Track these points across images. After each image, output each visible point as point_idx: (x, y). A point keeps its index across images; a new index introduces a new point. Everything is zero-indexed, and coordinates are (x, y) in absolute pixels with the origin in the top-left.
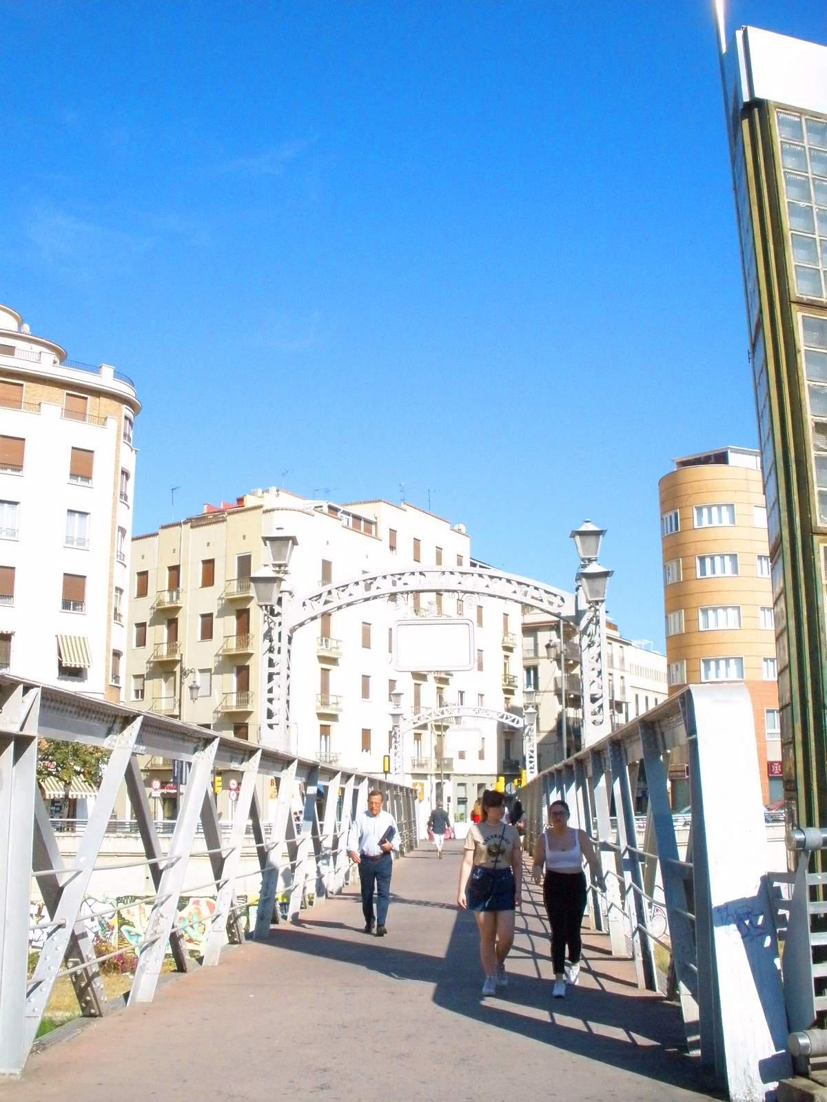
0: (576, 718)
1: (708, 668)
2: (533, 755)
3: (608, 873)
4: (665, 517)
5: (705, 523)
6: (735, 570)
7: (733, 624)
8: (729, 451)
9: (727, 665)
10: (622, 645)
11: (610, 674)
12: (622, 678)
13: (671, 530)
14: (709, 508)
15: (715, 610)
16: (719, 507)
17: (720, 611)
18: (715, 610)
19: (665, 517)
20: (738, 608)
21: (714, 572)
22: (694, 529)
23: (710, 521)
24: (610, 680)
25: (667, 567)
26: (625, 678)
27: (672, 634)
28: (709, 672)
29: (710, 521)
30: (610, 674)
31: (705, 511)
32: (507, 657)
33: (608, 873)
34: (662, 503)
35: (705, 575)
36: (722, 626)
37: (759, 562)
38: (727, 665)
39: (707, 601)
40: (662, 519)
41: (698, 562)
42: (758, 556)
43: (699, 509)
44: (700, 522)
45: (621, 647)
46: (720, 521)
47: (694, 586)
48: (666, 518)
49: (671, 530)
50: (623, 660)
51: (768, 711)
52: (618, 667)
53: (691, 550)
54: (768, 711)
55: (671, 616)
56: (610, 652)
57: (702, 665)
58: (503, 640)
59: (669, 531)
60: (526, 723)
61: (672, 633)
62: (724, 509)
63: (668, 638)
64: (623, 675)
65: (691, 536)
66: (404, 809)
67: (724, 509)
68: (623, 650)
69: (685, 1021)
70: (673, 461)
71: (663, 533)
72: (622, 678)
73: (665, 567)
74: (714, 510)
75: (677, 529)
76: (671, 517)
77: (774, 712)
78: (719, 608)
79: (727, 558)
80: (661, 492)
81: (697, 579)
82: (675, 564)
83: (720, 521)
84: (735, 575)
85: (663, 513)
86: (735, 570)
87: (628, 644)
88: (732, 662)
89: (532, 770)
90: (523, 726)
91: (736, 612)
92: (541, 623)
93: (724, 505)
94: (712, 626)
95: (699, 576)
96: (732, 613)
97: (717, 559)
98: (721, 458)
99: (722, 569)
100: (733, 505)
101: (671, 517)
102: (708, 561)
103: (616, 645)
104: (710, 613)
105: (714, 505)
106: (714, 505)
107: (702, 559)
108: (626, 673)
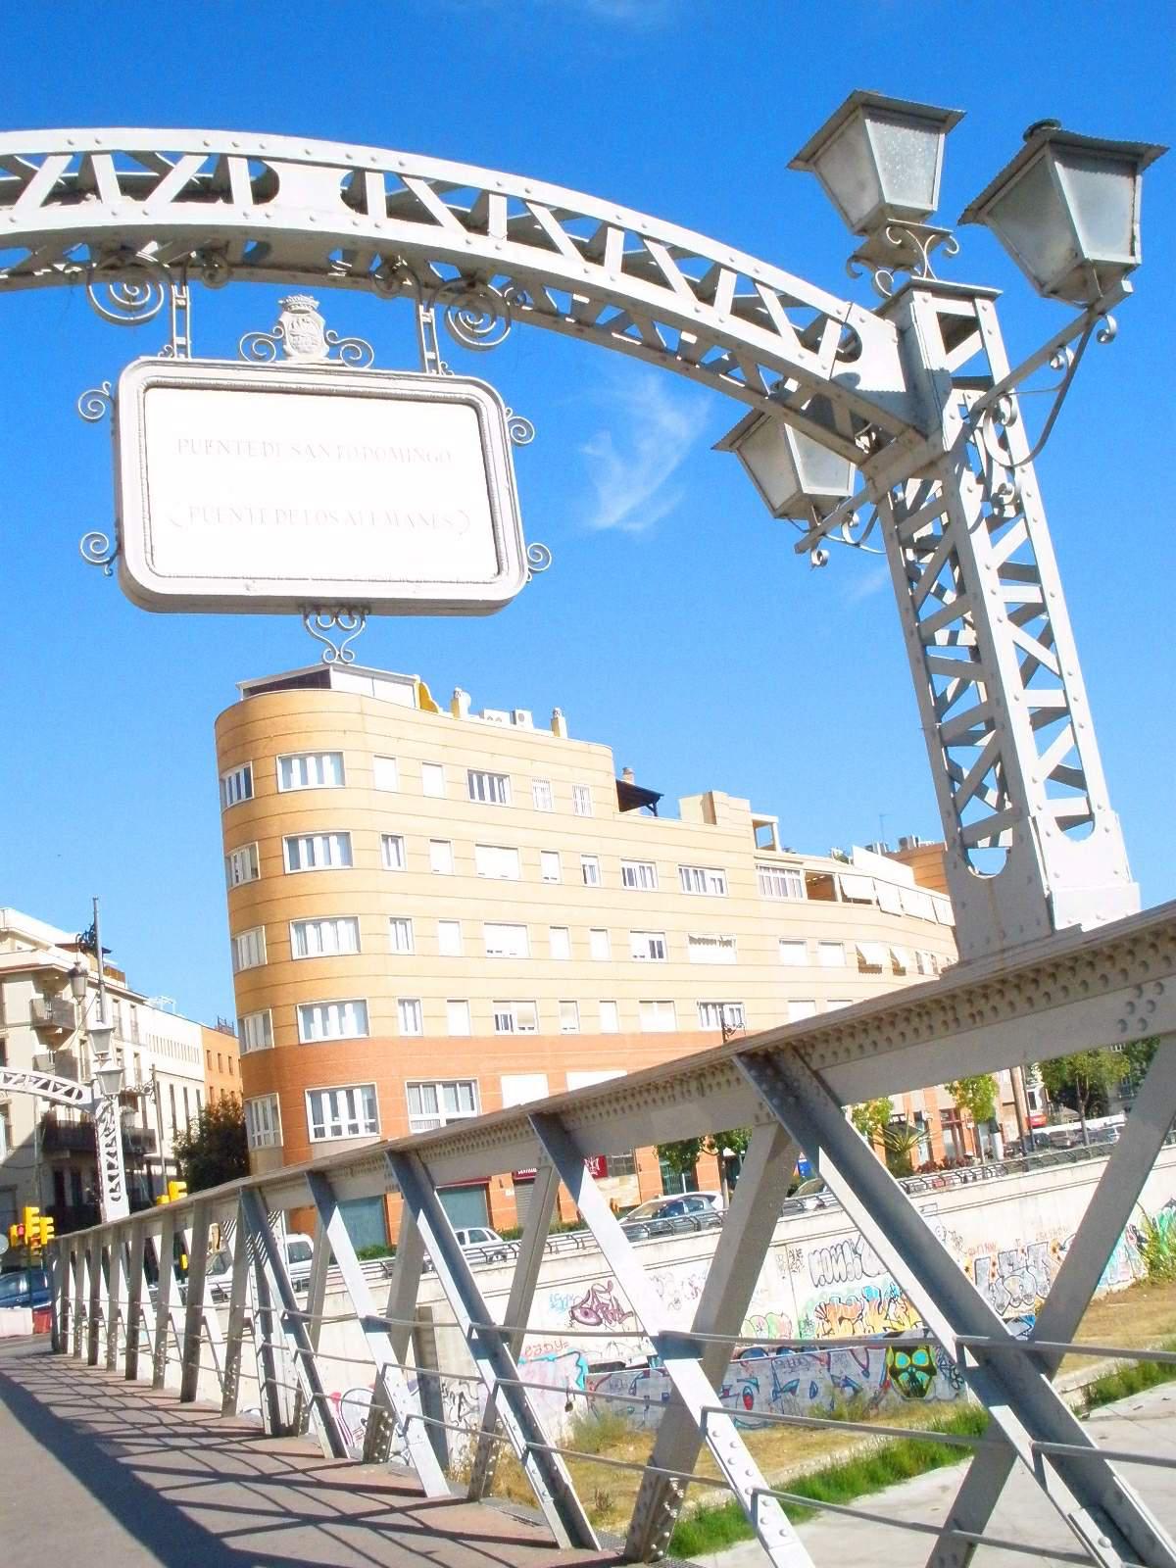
0: (70, 1121)
1: (309, 1019)
2: (110, 1159)
3: (754, 1497)
4: (226, 777)
5: (296, 783)
6: (348, 858)
7: (348, 946)
8: (331, 669)
9: (342, 1013)
10: (134, 1004)
11: (119, 1050)
12: (136, 1055)
13: (239, 797)
14: (303, 759)
15: (317, 923)
16: (319, 756)
17: (325, 926)
18: (317, 923)
19: (226, 777)
20: (355, 919)
21: (312, 862)
22: (279, 793)
23: (305, 779)
24: (119, 1060)
25: (233, 860)
26: (141, 1056)
27: (245, 967)
28: (312, 1025)
29: (305, 779)
30: (119, 1050)
31: (296, 763)
33: (754, 1497)
34: (223, 754)
35: (299, 868)
36: (330, 949)
37: (384, 845)
38: (342, 1013)
39: (305, 910)
40: (222, 781)
41: (286, 846)
42: (383, 835)
43: (287, 761)
44: (288, 783)
45: (133, 1007)
46: (321, 780)
47: (280, 887)
48: (230, 778)
49: (239, 797)
50: (136, 1026)
51: (411, 1086)
52: (130, 1039)
53: (274, 827)
54: (411, 1086)
55: (242, 939)
56: (116, 1014)
57: (300, 1015)
59: (228, 802)
60: (98, 1096)
61: (245, 965)
62: (326, 759)
63: (238, 974)
64: (137, 1052)
65: (274, 805)
66: (1056, 1448)
67: (326, 759)
68: (135, 1011)
69: (31, 982)
70: (238, 686)
71: (224, 802)
72: (136, 1055)
73: (228, 858)
74: (311, 761)
75: (249, 794)
76: (238, 776)
77: (418, 1087)
78: (339, 919)
79: (333, 840)
80: (219, 738)
81: (285, 875)
82: (247, 852)
83: (321, 780)
84: (348, 867)
85: (222, 771)
86: (348, 858)
87: (141, 1002)
88: (349, 1007)
89: (115, 1195)
90: (90, 1101)
91: (351, 925)
92: (12, 968)
93: (327, 753)
94: (313, 952)
95: (288, 870)
96: (345, 928)
97: (318, 842)
98: (318, 680)
99: (325, 856)
100: (341, 753)
101: (238, 776)
102: (302, 845)
103: (125, 1003)
104: (310, 928)
105: (310, 754)
106: (310, 754)
107: (293, 842)
108: (142, 1047)
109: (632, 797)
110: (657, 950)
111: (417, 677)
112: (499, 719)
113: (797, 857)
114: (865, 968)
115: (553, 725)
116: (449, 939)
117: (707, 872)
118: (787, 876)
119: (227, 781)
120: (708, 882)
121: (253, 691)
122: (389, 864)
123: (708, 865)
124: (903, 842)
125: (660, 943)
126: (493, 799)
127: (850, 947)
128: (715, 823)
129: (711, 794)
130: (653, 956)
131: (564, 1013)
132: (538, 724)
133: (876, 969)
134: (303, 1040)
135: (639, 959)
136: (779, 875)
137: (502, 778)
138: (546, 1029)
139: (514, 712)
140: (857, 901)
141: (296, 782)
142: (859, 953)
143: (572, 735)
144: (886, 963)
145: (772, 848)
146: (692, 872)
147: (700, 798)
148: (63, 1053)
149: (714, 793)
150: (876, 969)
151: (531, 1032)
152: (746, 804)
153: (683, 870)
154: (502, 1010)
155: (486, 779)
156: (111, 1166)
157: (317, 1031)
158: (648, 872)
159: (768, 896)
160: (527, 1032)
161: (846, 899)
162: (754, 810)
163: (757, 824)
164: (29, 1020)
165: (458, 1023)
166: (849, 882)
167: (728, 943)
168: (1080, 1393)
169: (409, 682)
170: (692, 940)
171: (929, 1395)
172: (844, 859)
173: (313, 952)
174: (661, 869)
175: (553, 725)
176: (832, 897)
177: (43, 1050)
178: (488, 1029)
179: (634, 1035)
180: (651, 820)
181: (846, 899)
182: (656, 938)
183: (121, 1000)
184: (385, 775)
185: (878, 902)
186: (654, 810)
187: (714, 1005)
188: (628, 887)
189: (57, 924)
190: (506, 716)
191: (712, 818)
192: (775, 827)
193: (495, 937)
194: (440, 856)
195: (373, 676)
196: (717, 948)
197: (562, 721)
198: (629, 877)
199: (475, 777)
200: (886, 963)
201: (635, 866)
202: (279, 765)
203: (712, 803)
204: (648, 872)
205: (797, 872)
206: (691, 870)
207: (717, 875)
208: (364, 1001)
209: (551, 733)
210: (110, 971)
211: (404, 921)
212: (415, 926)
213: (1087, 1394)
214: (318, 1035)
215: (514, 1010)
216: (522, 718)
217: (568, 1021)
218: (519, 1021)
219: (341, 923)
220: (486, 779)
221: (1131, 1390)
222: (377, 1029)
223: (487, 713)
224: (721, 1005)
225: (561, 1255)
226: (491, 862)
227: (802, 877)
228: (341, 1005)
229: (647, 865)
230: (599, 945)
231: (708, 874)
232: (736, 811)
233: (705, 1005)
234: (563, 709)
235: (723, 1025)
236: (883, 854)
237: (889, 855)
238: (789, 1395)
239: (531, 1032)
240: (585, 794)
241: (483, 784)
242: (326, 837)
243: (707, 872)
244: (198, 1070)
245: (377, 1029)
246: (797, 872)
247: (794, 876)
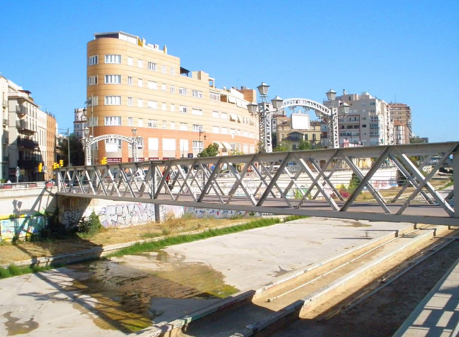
4: (90, 57)
6: (120, 81)
7: (118, 103)
9: (115, 119)
12: (36, 121)
13: (91, 63)
14: (111, 56)
15: (111, 97)
17: (113, 98)
18: (111, 97)
19: (90, 57)
21: (111, 82)
23: (111, 61)
32: (4, 111)
41: (105, 77)
43: (107, 56)
44: (107, 61)
49: (91, 63)
53: (103, 72)
57: (105, 119)
58: (3, 104)
59: (90, 63)
62: (117, 56)
67: (117, 56)
74: (113, 57)
75: (96, 62)
76: (94, 58)
79: (117, 77)
86: (120, 81)
88: (117, 118)
94: (110, 104)
95: (105, 83)
96: (118, 99)
97: (113, 77)
98: (116, 36)
99: (114, 81)
101: (94, 58)
102: (109, 77)
103: (35, 107)
104: (109, 98)
107: (107, 76)
109: (183, 71)
110: (185, 110)
111: (138, 37)
112: (151, 47)
113: (217, 89)
114: (232, 120)
115: (164, 49)
116: (140, 103)
117: (198, 92)
118: (216, 95)
119: (90, 59)
120: (198, 95)
121: (98, 37)
122: (129, 84)
123: (198, 90)
124: (242, 87)
125: (186, 109)
126: (153, 69)
127: (229, 114)
128: (200, 79)
129: (200, 71)
130: (184, 112)
131: (163, 123)
132: (160, 49)
133: (234, 121)
134: (105, 125)
135: (150, 108)
136: (214, 94)
137: (155, 64)
138: (159, 127)
139: (154, 45)
140: (232, 103)
141: (109, 62)
142: (231, 116)
143: (168, 53)
144: (236, 119)
145: (212, 86)
146: (195, 92)
147: (197, 72)
148: (22, 120)
149: (201, 71)
150: (234, 121)
151: (155, 128)
152: (208, 75)
153: (193, 91)
154: (150, 122)
155: (152, 64)
156: (88, 151)
157: (108, 123)
158: (185, 91)
159: (211, 99)
160: (155, 128)
161: (229, 102)
162: (210, 76)
163: (210, 80)
164: (15, 110)
165: (140, 124)
166: (230, 98)
167: (201, 110)
168: (283, 219)
169: (136, 38)
170: (193, 109)
171: (255, 215)
172: (228, 91)
173: (110, 104)
174: (188, 90)
175: (164, 49)
176: (226, 101)
177: (18, 119)
178: (147, 126)
179: (178, 131)
180: (186, 77)
181: (229, 102)
182: (185, 107)
183: (34, 107)
184: (130, 62)
185: (236, 104)
186: (187, 75)
187: (196, 125)
188: (180, 94)
189: (19, 85)
190: (153, 46)
191: (200, 78)
192: (214, 81)
193: (150, 104)
194: (140, 83)
195: (128, 36)
196: (198, 111)
197: (166, 49)
198: (181, 91)
199: (149, 63)
200: (236, 119)
201: (182, 89)
202: (105, 57)
203: (200, 74)
204: (185, 91)
205: (219, 94)
206: (195, 91)
207: (201, 93)
208: (121, 117)
209: (163, 51)
210: (30, 98)
211: (131, 98)
212: (133, 100)
213: (284, 219)
214: (109, 124)
215: (152, 122)
216: (156, 47)
217: (164, 126)
218: (154, 125)
219: (117, 97)
220: (152, 64)
221: (293, 220)
222: (123, 124)
223: (149, 45)
224: (198, 125)
225: (38, 187)
226: (151, 85)
227: (220, 96)
228: (115, 117)
229: (185, 89)
230: (173, 108)
231: (199, 92)
232: (205, 76)
233: (194, 125)
234: (166, 45)
235: (200, 131)
236: (236, 90)
237: (238, 90)
238: (226, 213)
239: (155, 128)
240: (173, 69)
241: (151, 65)
242: (115, 76)
243: (198, 92)
244: (45, 126)
245: (123, 124)
246: (219, 94)
247: (218, 95)
